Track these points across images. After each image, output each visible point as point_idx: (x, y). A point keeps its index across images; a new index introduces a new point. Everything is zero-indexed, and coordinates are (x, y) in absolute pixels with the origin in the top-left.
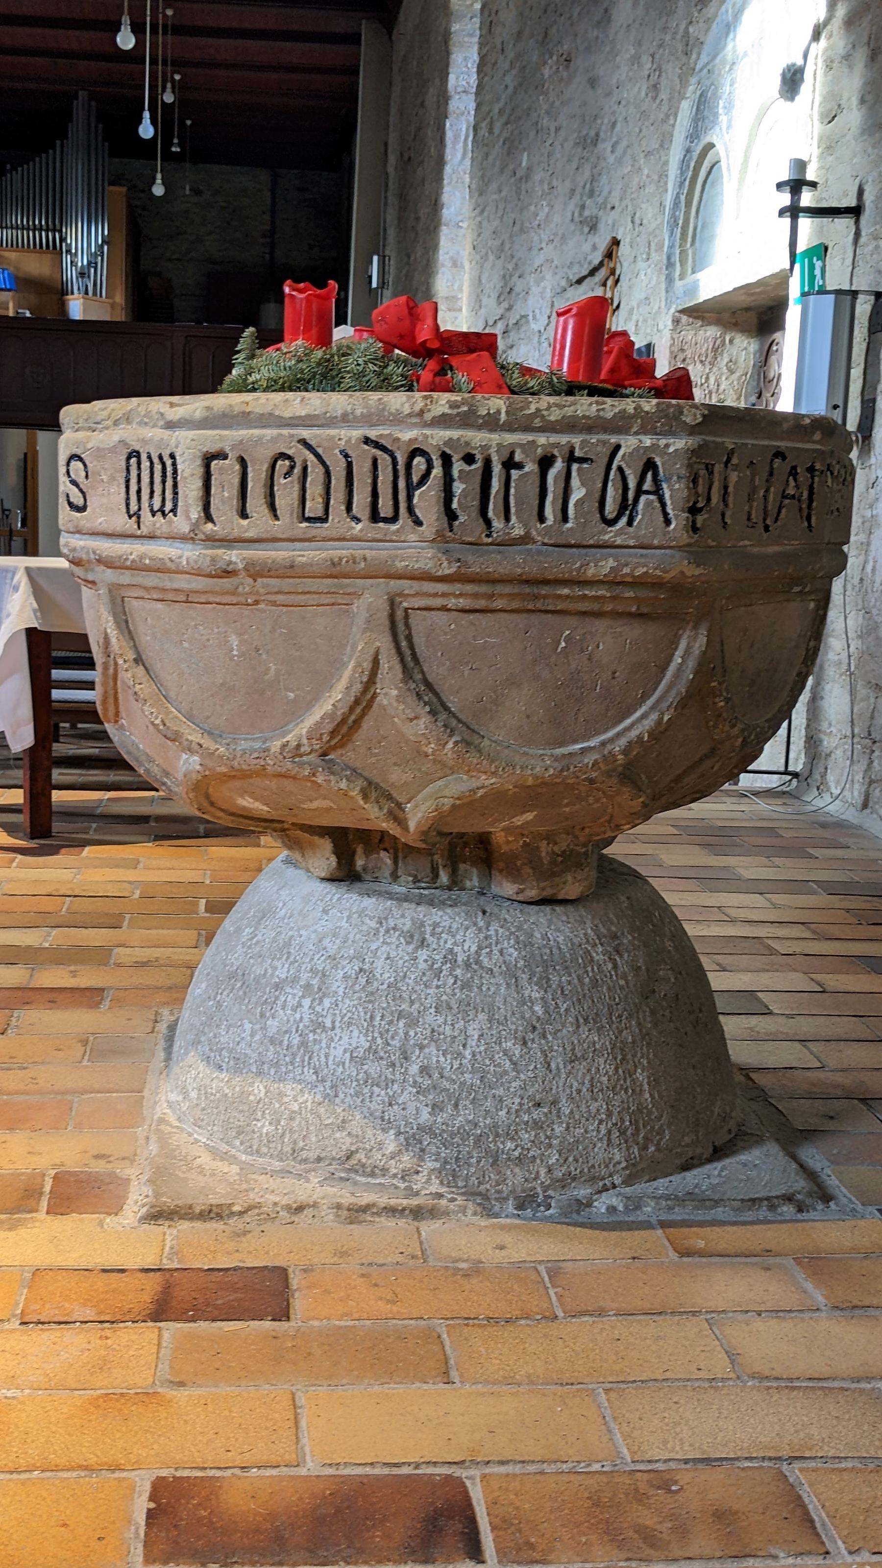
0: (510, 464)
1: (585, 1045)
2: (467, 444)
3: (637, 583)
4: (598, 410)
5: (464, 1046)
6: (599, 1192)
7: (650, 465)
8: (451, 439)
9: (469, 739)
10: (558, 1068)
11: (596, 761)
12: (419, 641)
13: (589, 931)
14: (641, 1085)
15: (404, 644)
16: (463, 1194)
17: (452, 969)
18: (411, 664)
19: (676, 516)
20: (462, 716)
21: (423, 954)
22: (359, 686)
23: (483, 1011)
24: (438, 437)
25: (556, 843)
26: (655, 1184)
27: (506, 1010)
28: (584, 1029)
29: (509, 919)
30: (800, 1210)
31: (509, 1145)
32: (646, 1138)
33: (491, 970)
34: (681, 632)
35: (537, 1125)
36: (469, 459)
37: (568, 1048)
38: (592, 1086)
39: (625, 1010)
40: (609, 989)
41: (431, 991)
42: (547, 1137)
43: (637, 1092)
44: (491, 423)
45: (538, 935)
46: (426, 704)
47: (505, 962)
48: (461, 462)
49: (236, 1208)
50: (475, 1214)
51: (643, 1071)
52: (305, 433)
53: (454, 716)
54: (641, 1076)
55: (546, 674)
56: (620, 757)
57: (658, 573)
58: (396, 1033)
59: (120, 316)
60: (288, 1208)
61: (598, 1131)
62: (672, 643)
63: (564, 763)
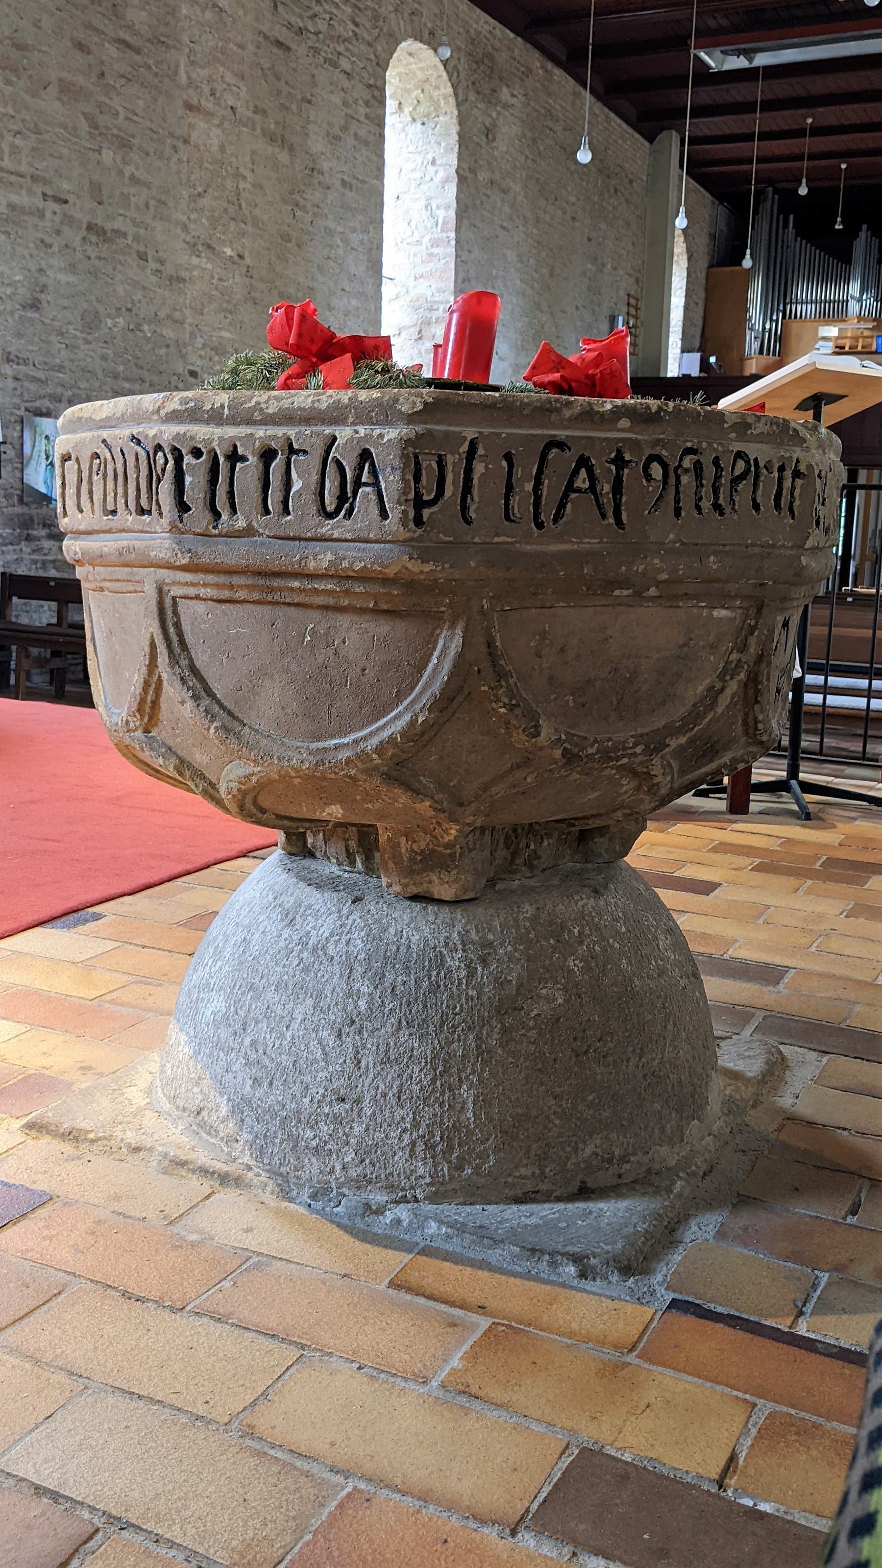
0: (234, 457)
2: (192, 438)
3: (362, 577)
4: (313, 402)
5: (288, 1027)
6: (397, 1202)
7: (365, 456)
8: (178, 434)
10: (367, 1067)
11: (348, 758)
13: (455, 935)
14: (464, 1103)
15: (172, 630)
16: (268, 1171)
17: (301, 951)
18: (178, 650)
19: (392, 509)
21: (286, 933)
22: (145, 668)
23: (311, 996)
24: (168, 433)
25: (414, 841)
26: (468, 1209)
27: (332, 999)
28: (404, 1033)
30: (583, 1275)
31: (309, 1134)
33: (332, 958)
34: (438, 631)
35: (337, 1120)
36: (197, 453)
37: (382, 1048)
38: (400, 1091)
40: (451, 997)
41: (278, 969)
42: (345, 1134)
44: (216, 417)
45: (392, 930)
46: (189, 689)
47: (347, 952)
48: (190, 456)
49: (91, 1136)
50: (272, 1193)
52: (105, 434)
53: (219, 703)
54: (465, 1093)
55: (294, 667)
57: (376, 567)
61: (400, 1139)
62: (428, 643)
63: (319, 757)
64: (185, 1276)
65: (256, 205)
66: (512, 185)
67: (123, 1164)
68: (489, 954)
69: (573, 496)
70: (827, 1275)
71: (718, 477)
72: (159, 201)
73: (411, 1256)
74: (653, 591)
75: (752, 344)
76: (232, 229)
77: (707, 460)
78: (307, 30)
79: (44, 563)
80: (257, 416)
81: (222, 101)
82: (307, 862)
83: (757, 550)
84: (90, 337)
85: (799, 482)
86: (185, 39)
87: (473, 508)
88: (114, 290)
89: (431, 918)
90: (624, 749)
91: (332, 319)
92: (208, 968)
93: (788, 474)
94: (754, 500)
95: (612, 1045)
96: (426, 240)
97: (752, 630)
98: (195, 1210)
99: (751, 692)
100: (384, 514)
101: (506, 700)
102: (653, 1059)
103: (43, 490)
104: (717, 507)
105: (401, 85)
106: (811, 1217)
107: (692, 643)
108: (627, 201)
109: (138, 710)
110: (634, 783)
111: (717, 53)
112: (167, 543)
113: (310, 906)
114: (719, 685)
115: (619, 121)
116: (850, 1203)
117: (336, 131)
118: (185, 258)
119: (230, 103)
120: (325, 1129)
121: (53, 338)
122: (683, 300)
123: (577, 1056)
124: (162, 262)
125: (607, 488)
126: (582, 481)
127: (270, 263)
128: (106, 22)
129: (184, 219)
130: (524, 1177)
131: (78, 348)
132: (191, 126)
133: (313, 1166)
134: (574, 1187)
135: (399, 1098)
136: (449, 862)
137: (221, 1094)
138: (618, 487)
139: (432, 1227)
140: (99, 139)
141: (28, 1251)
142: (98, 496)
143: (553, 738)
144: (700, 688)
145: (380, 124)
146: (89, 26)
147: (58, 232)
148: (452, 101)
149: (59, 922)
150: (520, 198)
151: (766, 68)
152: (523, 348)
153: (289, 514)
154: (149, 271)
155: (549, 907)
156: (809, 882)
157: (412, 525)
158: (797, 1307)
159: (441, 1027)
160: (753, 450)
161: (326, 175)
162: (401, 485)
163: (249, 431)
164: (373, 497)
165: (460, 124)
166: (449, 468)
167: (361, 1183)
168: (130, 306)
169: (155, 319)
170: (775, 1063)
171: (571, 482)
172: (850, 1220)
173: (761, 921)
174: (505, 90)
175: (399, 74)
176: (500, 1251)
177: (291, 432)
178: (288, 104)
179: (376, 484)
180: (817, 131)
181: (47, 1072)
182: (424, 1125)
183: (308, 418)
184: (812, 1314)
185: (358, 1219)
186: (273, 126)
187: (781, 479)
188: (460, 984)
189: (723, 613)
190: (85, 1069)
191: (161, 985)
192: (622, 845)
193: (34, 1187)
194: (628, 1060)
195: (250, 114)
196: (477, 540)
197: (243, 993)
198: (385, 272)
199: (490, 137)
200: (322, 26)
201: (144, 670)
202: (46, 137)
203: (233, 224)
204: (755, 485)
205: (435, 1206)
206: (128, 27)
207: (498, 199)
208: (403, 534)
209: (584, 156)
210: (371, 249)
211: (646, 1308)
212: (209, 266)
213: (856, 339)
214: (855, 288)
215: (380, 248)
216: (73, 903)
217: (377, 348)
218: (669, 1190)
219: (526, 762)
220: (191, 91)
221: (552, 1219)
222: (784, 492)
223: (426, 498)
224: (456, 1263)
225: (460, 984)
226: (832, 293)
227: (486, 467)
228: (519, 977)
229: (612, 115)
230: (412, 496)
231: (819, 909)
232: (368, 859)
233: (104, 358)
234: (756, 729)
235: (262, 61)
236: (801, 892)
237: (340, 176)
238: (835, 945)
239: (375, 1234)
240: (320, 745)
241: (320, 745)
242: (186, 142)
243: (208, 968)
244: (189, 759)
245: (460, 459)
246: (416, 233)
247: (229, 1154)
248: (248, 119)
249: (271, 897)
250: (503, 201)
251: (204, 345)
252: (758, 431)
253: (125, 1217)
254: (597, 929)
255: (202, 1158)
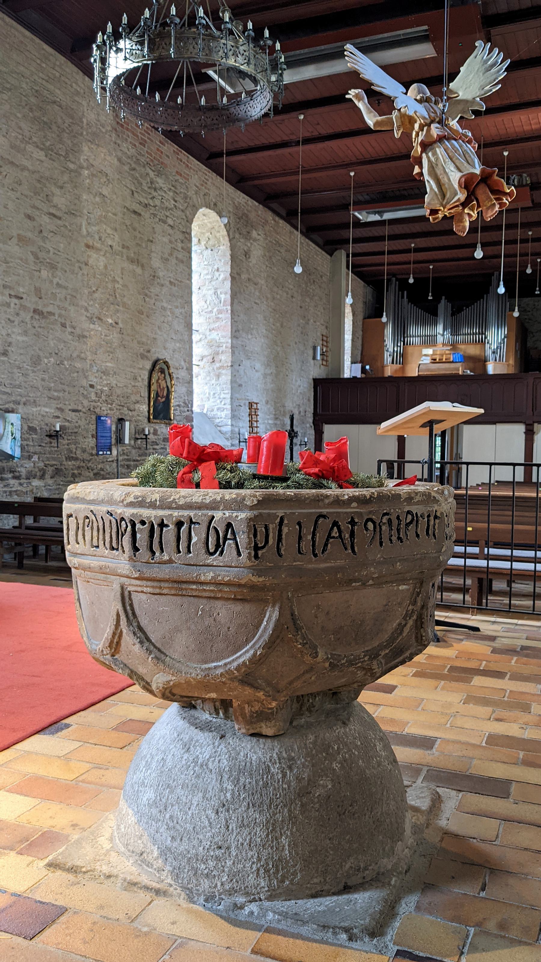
0: (162, 525)
1: (250, 819)
2: (141, 516)
3: (228, 584)
6: (250, 902)
7: (229, 525)
9: (159, 657)
10: (233, 830)
11: (222, 673)
12: (136, 606)
13: (275, 755)
14: (284, 846)
15: (128, 608)
16: (181, 887)
17: (194, 767)
20: (157, 645)
21: (186, 756)
24: (128, 512)
25: (252, 706)
26: (288, 903)
28: (251, 810)
29: (231, 743)
30: (350, 939)
31: (203, 866)
32: (283, 876)
35: (218, 858)
36: (143, 523)
38: (250, 842)
39: (282, 802)
40: (275, 789)
41: (183, 776)
42: (222, 866)
43: (279, 849)
44: (152, 505)
45: (242, 754)
49: (84, 870)
51: (286, 838)
52: (92, 507)
54: (284, 841)
55: (193, 627)
56: (235, 672)
57: (235, 579)
58: (165, 795)
59: (511, 371)
60: (105, 874)
61: (251, 868)
63: (206, 672)
64: (144, 954)
65: (124, 296)
66: (260, 281)
67: (102, 885)
68: (293, 764)
69: (331, 540)
70: (473, 929)
71: (399, 524)
72: (72, 296)
73: (261, 933)
74: (371, 582)
75: (388, 358)
76: (112, 309)
77: (394, 518)
78: (150, 205)
79: (10, 492)
80: (174, 505)
81: (105, 243)
82: (193, 712)
83: (419, 556)
84: (35, 369)
85: (437, 521)
86: (85, 212)
87: (283, 549)
88: (48, 344)
89: (262, 746)
90: (360, 659)
91: (166, 354)
92: (143, 773)
93: (432, 518)
94: (416, 533)
95: (357, 808)
96: (215, 310)
97: (418, 594)
98: (144, 912)
99: (419, 623)
100: (239, 554)
101: (301, 641)
102: (377, 812)
103: (10, 452)
104: (399, 538)
105: (200, 230)
106: (462, 894)
107: (390, 604)
108: (320, 287)
109: (109, 646)
110: (363, 672)
111: (364, 213)
112: (127, 567)
113: (197, 741)
114: (403, 623)
115: (314, 245)
116: (481, 884)
117: (166, 256)
118: (86, 325)
119: (109, 243)
120: (211, 864)
121: (15, 370)
122: (351, 336)
123: (340, 815)
124: (74, 328)
125: (347, 536)
126: (335, 533)
127: (132, 326)
128: (43, 204)
129: (86, 304)
130: (316, 884)
131: (28, 375)
132: (89, 256)
133: (205, 884)
134: (341, 887)
135: (250, 845)
136: (270, 717)
137: (154, 845)
138: (352, 534)
139: (270, 916)
140: (39, 264)
141: (59, 944)
142: (88, 537)
143: (325, 657)
144: (395, 625)
145: (189, 251)
146: (34, 207)
147: (18, 314)
148: (227, 238)
149: (47, 731)
150: (264, 287)
151: (389, 220)
152: (268, 365)
153: (190, 553)
154: (67, 333)
155: (321, 735)
156: (443, 682)
157: (253, 559)
158: (459, 949)
159: (270, 806)
160: (414, 509)
161: (162, 279)
162: (247, 540)
163: (170, 513)
164: (234, 546)
165: (231, 250)
166: (271, 530)
167: (231, 892)
168: (57, 352)
169: (71, 358)
170: (435, 800)
171: (330, 534)
172: (483, 894)
173: (420, 709)
174: (254, 232)
175: (199, 225)
176: (307, 928)
177: (192, 514)
178: (140, 243)
179: (235, 539)
180: (416, 250)
181: (54, 829)
182: (263, 859)
183: (200, 507)
184: (468, 953)
185: (231, 913)
186: (132, 255)
187: (428, 521)
188: (279, 782)
189: (404, 587)
190: (74, 826)
191: (108, 769)
192: (355, 694)
193: (56, 903)
194: (365, 815)
195: (120, 249)
196: (285, 564)
197: (164, 789)
198: (194, 328)
199: (247, 256)
200: (158, 202)
201: (113, 627)
202: (11, 264)
203: (112, 306)
204: (417, 526)
205: (270, 903)
206: (55, 206)
207: (252, 288)
208: (249, 563)
209: (298, 269)
210: (186, 317)
211: (384, 957)
212: (100, 329)
213: (442, 355)
214: (440, 329)
215: (191, 316)
216: (53, 719)
217: (226, 456)
218: (389, 884)
219: (311, 669)
220: (88, 238)
221: (332, 906)
222: (430, 527)
223: (259, 545)
224: (285, 936)
225: (279, 782)
226: (428, 331)
227: (289, 529)
228: (309, 776)
229: (311, 243)
230: (253, 545)
231: (449, 700)
232: (226, 712)
233: (43, 380)
234: (422, 639)
235: (126, 222)
236: (439, 689)
237: (169, 279)
238: (459, 722)
239: (241, 921)
240: (207, 666)
241: (207, 666)
242: (86, 264)
243: (143, 773)
244: (135, 670)
245: (276, 526)
246: (209, 307)
247: (159, 877)
248: (120, 251)
249: (176, 735)
250: (255, 289)
251: (98, 371)
252: (417, 500)
253: (108, 919)
254: (346, 745)
255: (145, 880)
